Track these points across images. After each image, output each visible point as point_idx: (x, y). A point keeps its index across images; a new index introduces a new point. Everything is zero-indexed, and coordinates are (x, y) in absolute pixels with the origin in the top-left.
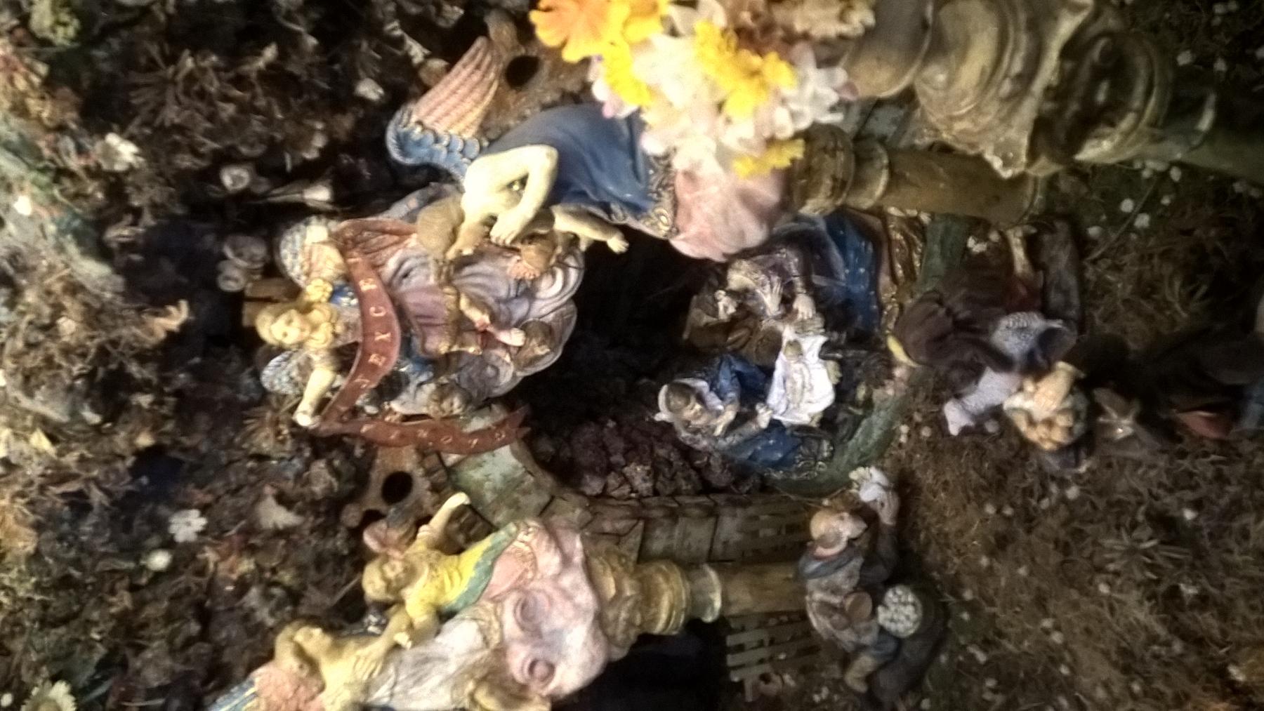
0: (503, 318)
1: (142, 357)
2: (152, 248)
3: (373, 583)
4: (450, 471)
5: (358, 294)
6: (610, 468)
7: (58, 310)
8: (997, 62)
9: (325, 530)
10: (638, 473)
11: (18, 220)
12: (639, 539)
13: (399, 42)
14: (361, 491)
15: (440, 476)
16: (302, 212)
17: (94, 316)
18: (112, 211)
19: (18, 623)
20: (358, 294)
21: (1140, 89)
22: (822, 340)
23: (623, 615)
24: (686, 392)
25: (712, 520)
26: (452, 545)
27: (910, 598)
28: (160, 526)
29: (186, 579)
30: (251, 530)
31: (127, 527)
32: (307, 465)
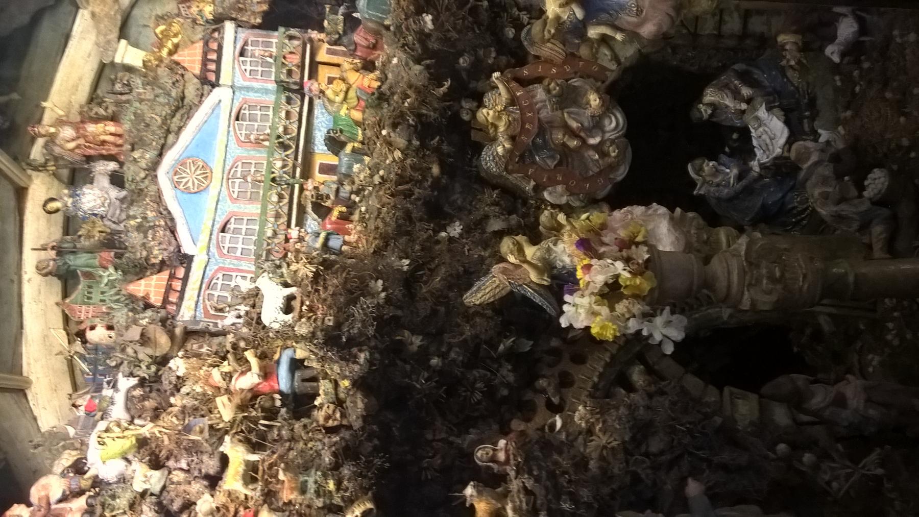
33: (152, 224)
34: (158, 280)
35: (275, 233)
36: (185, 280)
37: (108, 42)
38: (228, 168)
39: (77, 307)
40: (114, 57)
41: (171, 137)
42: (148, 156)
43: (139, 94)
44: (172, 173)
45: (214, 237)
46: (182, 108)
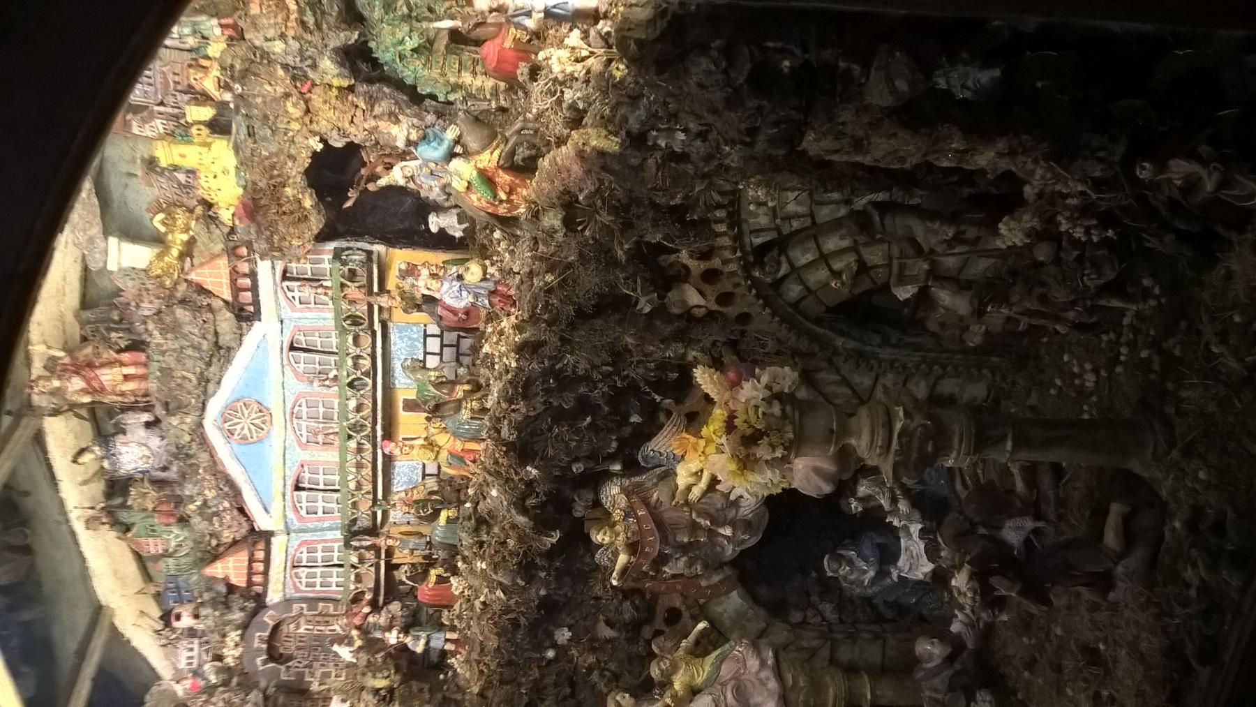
0: (721, 520)
1: (541, 555)
3: (655, 672)
4: (701, 607)
5: (637, 517)
6: (810, 605)
7: (507, 536)
8: (872, 441)
9: (633, 640)
10: (828, 609)
11: (492, 497)
12: (828, 652)
13: (649, 394)
14: (649, 617)
15: (696, 611)
16: (608, 475)
17: (521, 539)
19: (491, 682)
20: (637, 517)
21: (956, 440)
22: (920, 526)
23: (802, 698)
24: (839, 559)
25: (880, 642)
26: (701, 649)
27: (988, 698)
28: (550, 636)
29: (563, 664)
30: (594, 639)
31: (536, 637)
32: (621, 603)
33: (214, 509)
34: (236, 561)
35: (359, 486)
36: (267, 561)
37: (91, 240)
38: (289, 406)
39: (143, 540)
40: (106, 263)
41: (211, 387)
42: (188, 420)
43: (158, 345)
44: (220, 421)
45: (288, 497)
46: (221, 353)
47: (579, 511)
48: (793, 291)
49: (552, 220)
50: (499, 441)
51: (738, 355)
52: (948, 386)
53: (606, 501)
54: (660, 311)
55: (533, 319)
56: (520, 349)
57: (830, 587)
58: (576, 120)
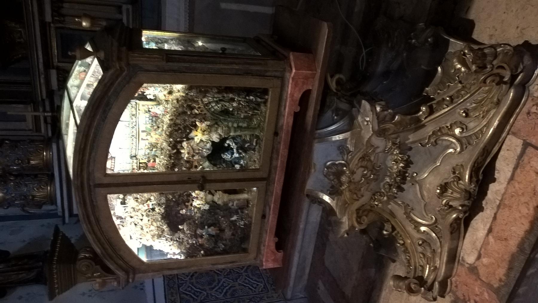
2: (173, 145)
16: (183, 141)
17: (169, 151)
18: (532, 256)
24: (224, 154)
47: (179, 147)
48: (213, 110)
49: (175, 101)
50: (166, 134)
51: (203, 119)
52: (240, 124)
53: (183, 145)
54: (191, 113)
55: (172, 115)
56: (170, 120)
57: (224, 161)
58: (179, 91)
